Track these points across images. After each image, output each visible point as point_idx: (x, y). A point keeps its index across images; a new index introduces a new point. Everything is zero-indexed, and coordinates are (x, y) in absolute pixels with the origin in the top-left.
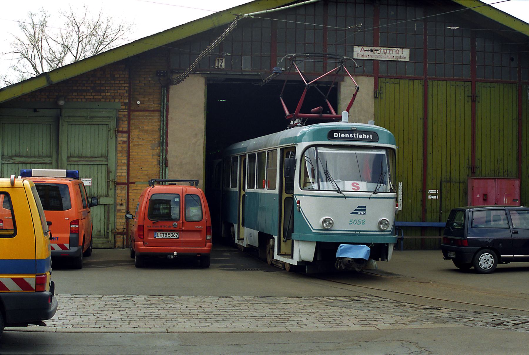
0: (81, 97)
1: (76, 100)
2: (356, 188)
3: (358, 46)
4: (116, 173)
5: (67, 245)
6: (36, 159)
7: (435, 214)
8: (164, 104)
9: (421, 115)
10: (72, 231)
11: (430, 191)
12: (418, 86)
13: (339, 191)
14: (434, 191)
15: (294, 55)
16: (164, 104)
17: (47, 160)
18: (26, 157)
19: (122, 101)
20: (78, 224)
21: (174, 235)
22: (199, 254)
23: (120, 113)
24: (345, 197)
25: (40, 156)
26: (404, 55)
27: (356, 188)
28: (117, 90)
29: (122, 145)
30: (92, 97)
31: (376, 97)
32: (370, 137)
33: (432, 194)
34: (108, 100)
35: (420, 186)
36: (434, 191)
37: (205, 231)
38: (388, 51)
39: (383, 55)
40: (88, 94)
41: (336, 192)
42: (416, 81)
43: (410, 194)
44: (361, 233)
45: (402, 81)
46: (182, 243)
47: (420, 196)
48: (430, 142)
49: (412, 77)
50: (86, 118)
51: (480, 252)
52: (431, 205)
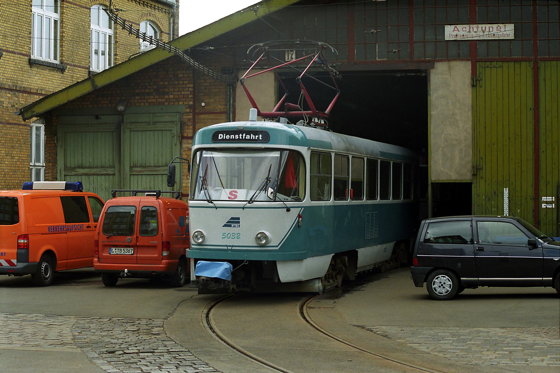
0: (144, 101)
1: (138, 104)
2: (233, 197)
3: (451, 25)
4: (181, 183)
5: (14, 261)
6: (99, 170)
7: (551, 226)
8: (230, 105)
9: (531, 104)
10: (19, 246)
11: (544, 199)
12: (526, 69)
13: (210, 201)
14: (549, 199)
15: (261, 44)
16: (230, 105)
17: (110, 171)
18: (90, 168)
19: (186, 103)
20: (28, 239)
21: (129, 251)
22: (154, 272)
23: (185, 117)
24: (216, 208)
25: (102, 167)
26: (507, 31)
27: (233, 197)
28: (181, 92)
29: (187, 153)
30: (154, 100)
31: (473, 86)
32: (258, 138)
33: (547, 202)
34: (172, 103)
35: (531, 192)
36: (549, 199)
37: (160, 246)
38: (487, 30)
39: (482, 34)
40: (151, 97)
41: (206, 202)
42: (523, 63)
43: (519, 203)
44: (233, 248)
45: (506, 64)
46: (137, 260)
47: (531, 204)
48: (542, 138)
49: (517, 58)
50: (149, 123)
51: (433, 274)
52: (546, 215)
